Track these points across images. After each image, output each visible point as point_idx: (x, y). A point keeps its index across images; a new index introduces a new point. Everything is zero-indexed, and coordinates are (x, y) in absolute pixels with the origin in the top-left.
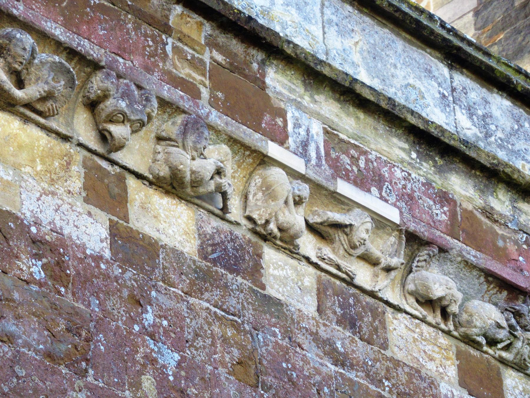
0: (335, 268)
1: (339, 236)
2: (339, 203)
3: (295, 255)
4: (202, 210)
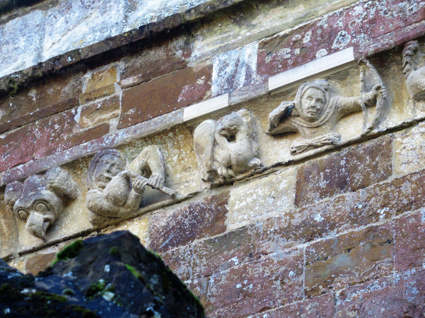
0: (312, 149)
1: (295, 123)
2: (285, 95)
3: (266, 172)
4: (156, 212)
